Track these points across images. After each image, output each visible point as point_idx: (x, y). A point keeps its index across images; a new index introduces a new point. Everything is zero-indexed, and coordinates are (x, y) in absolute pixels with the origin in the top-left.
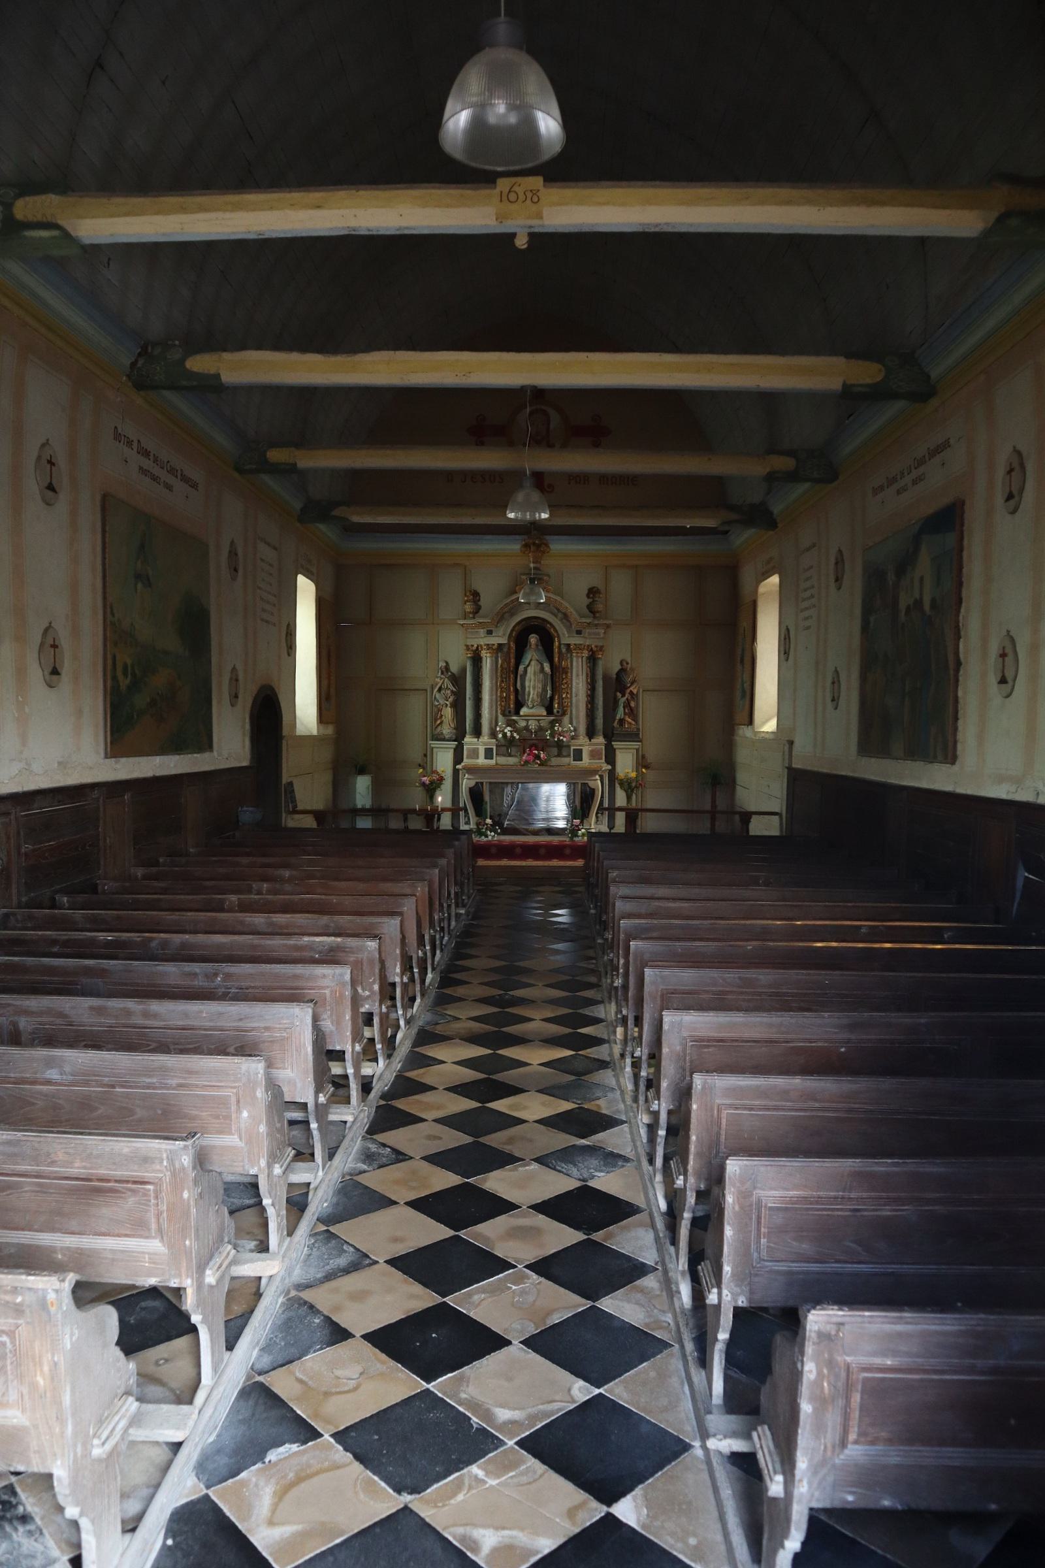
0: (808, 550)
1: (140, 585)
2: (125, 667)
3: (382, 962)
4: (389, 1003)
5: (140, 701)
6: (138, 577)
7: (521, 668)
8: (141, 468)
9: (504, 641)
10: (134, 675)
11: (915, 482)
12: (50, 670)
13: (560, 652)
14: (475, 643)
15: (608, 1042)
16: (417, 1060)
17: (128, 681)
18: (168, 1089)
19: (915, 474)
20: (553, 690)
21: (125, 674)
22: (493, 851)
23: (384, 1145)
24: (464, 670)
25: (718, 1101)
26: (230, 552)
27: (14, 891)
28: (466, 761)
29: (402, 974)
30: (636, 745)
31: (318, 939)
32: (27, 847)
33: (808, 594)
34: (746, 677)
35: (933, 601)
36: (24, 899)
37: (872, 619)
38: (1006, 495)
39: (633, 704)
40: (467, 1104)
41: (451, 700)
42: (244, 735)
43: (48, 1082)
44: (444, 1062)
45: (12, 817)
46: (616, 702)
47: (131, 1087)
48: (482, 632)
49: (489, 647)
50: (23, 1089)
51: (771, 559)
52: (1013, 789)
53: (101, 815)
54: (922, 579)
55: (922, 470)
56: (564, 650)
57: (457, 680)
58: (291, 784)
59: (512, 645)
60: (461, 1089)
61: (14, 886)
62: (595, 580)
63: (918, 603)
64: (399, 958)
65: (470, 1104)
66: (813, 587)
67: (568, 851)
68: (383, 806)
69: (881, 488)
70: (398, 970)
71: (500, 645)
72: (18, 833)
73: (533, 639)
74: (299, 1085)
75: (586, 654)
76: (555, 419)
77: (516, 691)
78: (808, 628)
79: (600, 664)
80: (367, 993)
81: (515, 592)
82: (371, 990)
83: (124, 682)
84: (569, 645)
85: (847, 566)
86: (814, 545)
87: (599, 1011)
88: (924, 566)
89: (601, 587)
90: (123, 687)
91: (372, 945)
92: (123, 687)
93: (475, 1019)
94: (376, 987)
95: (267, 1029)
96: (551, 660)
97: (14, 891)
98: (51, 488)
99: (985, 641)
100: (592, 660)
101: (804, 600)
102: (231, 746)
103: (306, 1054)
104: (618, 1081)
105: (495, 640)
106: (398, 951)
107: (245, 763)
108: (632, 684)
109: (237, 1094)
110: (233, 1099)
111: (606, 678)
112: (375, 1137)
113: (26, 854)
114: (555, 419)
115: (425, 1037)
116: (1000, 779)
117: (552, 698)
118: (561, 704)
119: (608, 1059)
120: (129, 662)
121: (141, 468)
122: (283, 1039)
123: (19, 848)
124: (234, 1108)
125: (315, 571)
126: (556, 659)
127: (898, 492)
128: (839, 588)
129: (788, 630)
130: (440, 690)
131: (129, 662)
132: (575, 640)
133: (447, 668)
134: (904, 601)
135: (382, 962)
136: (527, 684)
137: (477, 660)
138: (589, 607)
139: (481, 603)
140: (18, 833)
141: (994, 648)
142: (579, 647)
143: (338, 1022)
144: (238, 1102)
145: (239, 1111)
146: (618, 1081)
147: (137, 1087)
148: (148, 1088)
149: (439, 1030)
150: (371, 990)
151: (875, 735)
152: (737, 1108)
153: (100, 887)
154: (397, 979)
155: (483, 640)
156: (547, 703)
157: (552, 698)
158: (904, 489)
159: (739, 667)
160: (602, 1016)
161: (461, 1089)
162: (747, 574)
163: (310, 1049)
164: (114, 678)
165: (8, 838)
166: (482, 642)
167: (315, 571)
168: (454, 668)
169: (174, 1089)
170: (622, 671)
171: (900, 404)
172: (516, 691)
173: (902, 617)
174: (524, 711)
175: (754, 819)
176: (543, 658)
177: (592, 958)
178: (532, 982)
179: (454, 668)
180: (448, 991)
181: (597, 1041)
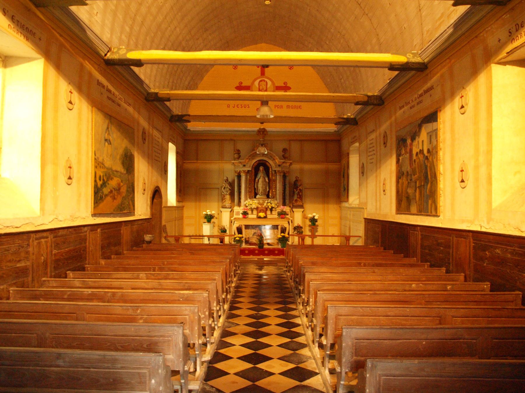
0: (371, 132)
1: (106, 143)
2: (100, 177)
3: (209, 302)
4: (212, 319)
5: (106, 191)
6: (106, 140)
7: (257, 179)
8: (108, 97)
9: (250, 169)
10: (103, 180)
11: (418, 104)
12: (68, 177)
13: (272, 174)
14: (238, 170)
15: (305, 335)
16: (223, 344)
17: (101, 182)
18: (116, 369)
19: (418, 100)
20: (269, 188)
21: (100, 180)
22: (247, 252)
23: (212, 387)
24: (234, 181)
25: (379, 372)
26: (143, 132)
27: (49, 270)
28: (235, 216)
29: (217, 306)
30: (302, 210)
31: (182, 292)
32: (55, 251)
33: (371, 150)
34: (346, 182)
35: (428, 150)
36: (53, 274)
37: (401, 158)
38: (460, 107)
39: (300, 194)
40: (248, 366)
41: (229, 192)
42: (147, 205)
43: (58, 366)
44: (234, 345)
45: (49, 239)
46: (294, 192)
47: (99, 368)
48: (241, 166)
49: (244, 171)
50: (44, 370)
51: (355, 136)
52: (469, 225)
53: (88, 237)
54: (423, 141)
55: (421, 99)
56: (274, 173)
57: (232, 185)
58: (165, 226)
59: (253, 171)
60: (244, 358)
61: (49, 268)
62: (284, 145)
63: (422, 151)
64: (215, 299)
65: (248, 366)
66: (374, 147)
67: (247, 252)
68: (201, 235)
69: (403, 106)
70: (215, 305)
71: (248, 171)
72: (52, 246)
73: (261, 168)
74: (176, 362)
75: (282, 174)
76: (269, 83)
77: (255, 189)
78: (372, 163)
79: (287, 179)
80: (203, 316)
81: (254, 150)
82: (205, 314)
83: (100, 183)
84: (275, 171)
85: (389, 138)
86: (374, 130)
87: (297, 321)
88: (424, 135)
89: (288, 148)
90: (99, 186)
91: (206, 295)
92: (99, 186)
93: (246, 325)
94: (207, 313)
95: (161, 336)
96: (268, 175)
97: (49, 270)
98: (70, 102)
99: (453, 165)
100: (284, 177)
101: (370, 152)
102: (142, 209)
103: (180, 347)
104: (312, 353)
105: (246, 169)
106: (215, 296)
107: (148, 217)
108: (300, 185)
109: (149, 371)
110: (148, 374)
111: (290, 183)
112: (208, 382)
113: (55, 254)
114: (269, 83)
115: (226, 333)
116: (463, 221)
117: (269, 192)
118: (272, 194)
119: (305, 343)
120: (102, 175)
121: (108, 97)
122: (169, 341)
123: (52, 251)
124: (148, 378)
125: (175, 141)
126: (270, 176)
127: (411, 108)
128: (385, 147)
129: (363, 164)
130: (224, 188)
131: (102, 175)
132: (278, 169)
133: (227, 180)
134: (415, 150)
135: (209, 302)
136: (259, 186)
137: (239, 177)
138: (283, 156)
139: (241, 154)
140: (52, 246)
141: (457, 168)
142: (279, 171)
143: (192, 330)
144: (150, 375)
145: (150, 380)
146: (312, 353)
147: (101, 368)
148: (106, 369)
149: (232, 330)
150: (205, 314)
151: (403, 203)
152: (388, 376)
153: (86, 268)
154: (215, 309)
155: (242, 169)
156: (267, 193)
157: (269, 192)
158: (413, 106)
159: (342, 179)
160: (300, 323)
161: (244, 358)
162: (345, 143)
163: (181, 345)
164: (95, 181)
165: (47, 248)
166: (241, 170)
167: (175, 141)
168: (230, 180)
169: (119, 369)
170: (296, 180)
171: (413, 72)
172: (255, 189)
173: (414, 157)
174: (258, 196)
175: (351, 238)
176: (266, 175)
177: (291, 297)
178: (268, 307)
179: (230, 180)
180: (234, 312)
181: (299, 335)
